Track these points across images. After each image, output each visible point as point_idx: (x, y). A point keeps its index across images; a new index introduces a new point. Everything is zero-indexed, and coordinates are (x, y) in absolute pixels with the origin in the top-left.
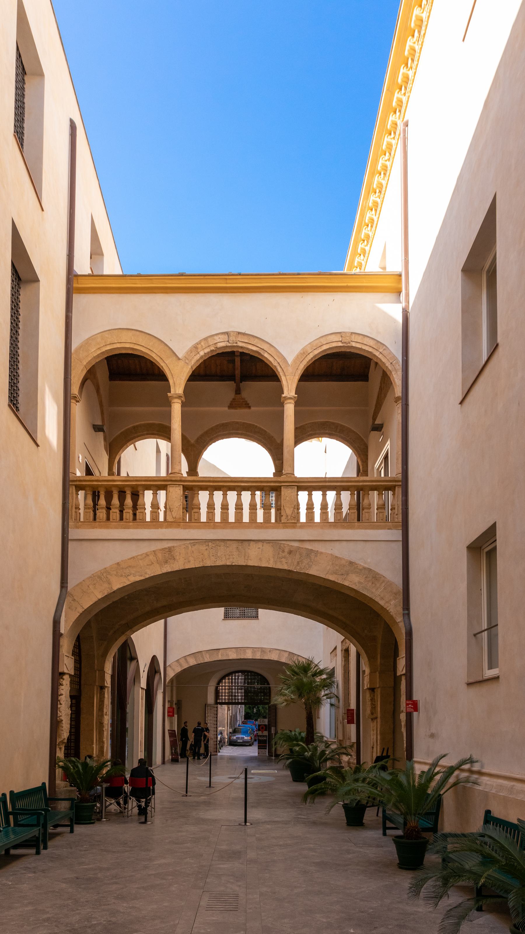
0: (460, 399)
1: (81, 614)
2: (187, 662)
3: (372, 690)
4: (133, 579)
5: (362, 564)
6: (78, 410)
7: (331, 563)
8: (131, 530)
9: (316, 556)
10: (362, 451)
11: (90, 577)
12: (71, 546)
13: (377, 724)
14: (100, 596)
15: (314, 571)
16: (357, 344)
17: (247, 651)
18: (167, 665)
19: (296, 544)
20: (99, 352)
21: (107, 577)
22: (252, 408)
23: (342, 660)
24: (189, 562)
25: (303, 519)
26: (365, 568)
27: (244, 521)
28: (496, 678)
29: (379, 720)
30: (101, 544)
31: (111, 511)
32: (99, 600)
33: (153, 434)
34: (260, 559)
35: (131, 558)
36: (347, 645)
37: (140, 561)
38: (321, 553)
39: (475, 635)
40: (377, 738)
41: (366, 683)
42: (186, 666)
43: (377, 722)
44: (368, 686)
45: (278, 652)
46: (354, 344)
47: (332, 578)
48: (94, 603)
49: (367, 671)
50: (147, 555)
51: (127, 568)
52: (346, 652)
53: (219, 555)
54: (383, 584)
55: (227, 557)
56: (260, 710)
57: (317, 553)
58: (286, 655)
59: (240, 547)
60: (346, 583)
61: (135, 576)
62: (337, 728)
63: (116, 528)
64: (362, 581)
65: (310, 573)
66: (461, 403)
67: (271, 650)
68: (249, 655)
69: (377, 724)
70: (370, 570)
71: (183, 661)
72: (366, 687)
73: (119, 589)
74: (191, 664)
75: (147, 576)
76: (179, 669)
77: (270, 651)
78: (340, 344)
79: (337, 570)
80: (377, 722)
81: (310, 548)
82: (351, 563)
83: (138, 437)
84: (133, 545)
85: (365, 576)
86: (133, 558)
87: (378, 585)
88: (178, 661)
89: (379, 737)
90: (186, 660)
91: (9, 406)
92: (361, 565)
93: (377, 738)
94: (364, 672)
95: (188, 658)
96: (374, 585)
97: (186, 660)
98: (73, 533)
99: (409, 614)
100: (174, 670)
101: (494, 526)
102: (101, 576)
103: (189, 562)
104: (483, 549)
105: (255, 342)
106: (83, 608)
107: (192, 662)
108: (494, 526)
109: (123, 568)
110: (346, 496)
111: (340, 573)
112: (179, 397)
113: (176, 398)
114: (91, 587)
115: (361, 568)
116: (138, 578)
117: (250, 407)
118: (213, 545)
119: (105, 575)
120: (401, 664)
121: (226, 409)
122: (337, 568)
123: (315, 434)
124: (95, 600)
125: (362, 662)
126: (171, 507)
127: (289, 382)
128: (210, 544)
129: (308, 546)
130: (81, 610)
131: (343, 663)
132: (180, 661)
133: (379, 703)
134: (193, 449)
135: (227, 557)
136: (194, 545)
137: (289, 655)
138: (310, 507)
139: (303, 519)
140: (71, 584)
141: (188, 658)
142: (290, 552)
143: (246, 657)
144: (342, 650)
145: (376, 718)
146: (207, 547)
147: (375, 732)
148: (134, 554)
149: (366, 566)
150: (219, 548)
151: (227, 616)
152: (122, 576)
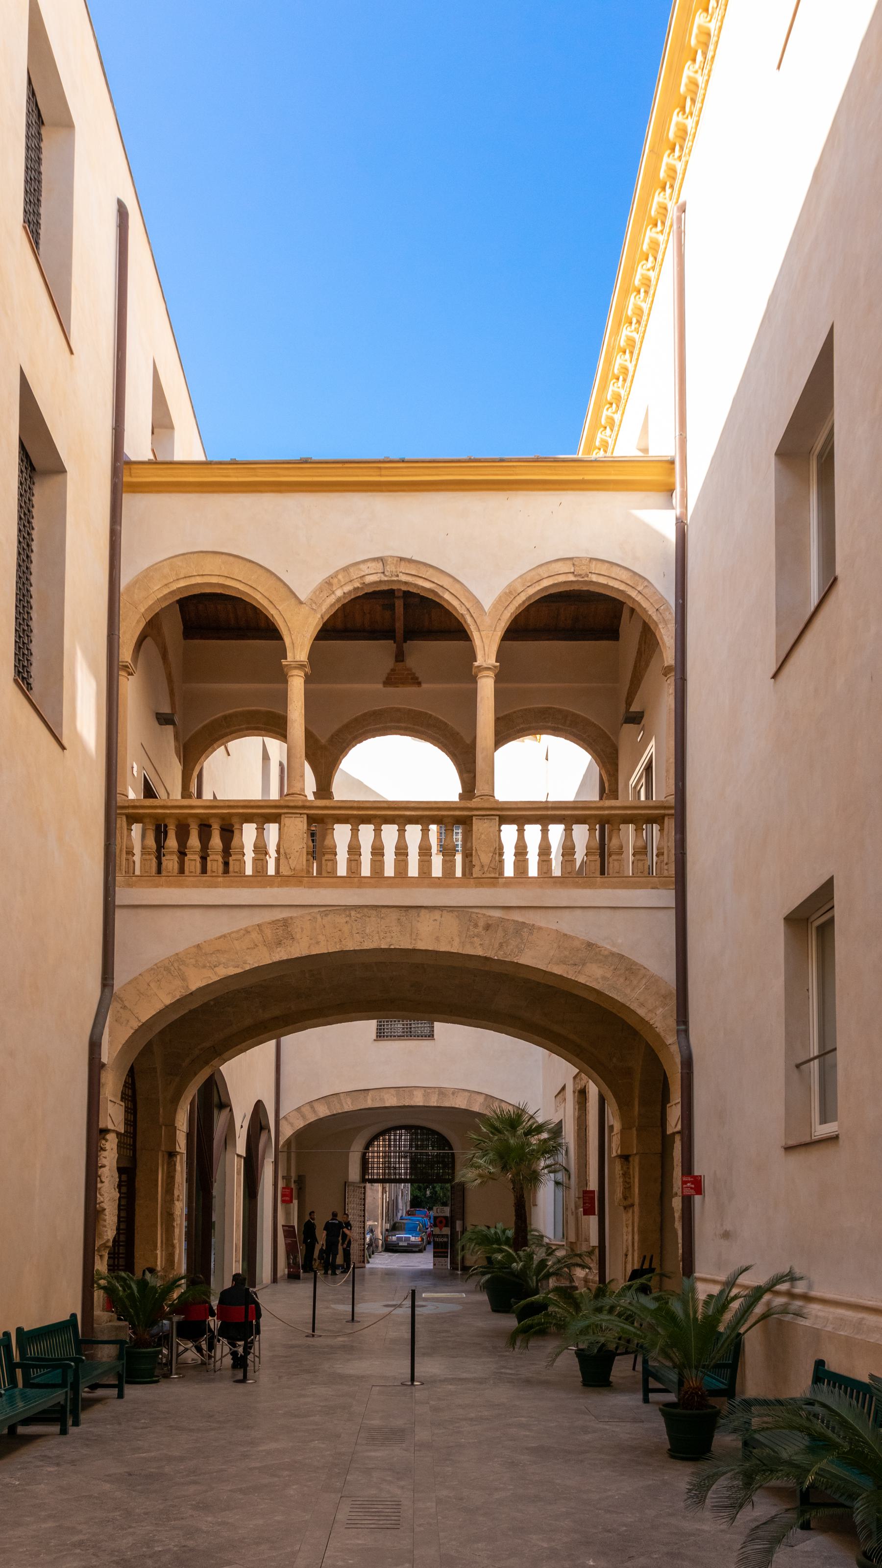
0: (774, 669)
1: (136, 1031)
2: (314, 1111)
3: (625, 1158)
4: (223, 972)
5: (608, 947)
6: (131, 688)
7: (555, 945)
8: (221, 890)
9: (531, 933)
10: (608, 758)
11: (152, 969)
12: (120, 916)
13: (633, 1216)
14: (168, 1001)
15: (527, 959)
16: (599, 578)
17: (415, 1093)
18: (281, 1116)
19: (497, 914)
20: (166, 591)
21: (180, 969)
22: (424, 686)
23: (575, 1109)
24: (318, 943)
25: (509, 871)
26: (613, 954)
27: (410, 875)
28: (833, 1139)
29: (636, 1208)
30: (170, 913)
31: (186, 858)
32: (167, 1007)
33: (257, 729)
34: (437, 939)
35: (220, 938)
36: (583, 1083)
37: (236, 942)
38: (540, 928)
39: (798, 1066)
40: (633, 1238)
41: (615, 1147)
42: (312, 1118)
43: (633, 1212)
44: (619, 1152)
45: (467, 1094)
46: (594, 578)
47: (557, 970)
48: (158, 1013)
49: (617, 1126)
50: (247, 931)
51: (213, 953)
52: (582, 1094)
53: (367, 931)
54: (644, 981)
55: (382, 935)
56: (436, 1192)
57: (532, 928)
58: (481, 1099)
59: (403, 919)
60: (582, 979)
61: (226, 966)
62: (567, 1222)
63: (195, 886)
64: (609, 975)
65: (521, 962)
66: (775, 676)
67: (455, 1092)
68: (418, 1100)
69: (633, 1216)
70: (621, 957)
71: (307, 1110)
72: (614, 1154)
73: (200, 989)
74: (322, 1115)
75: (247, 968)
76: (300, 1124)
77: (453, 1094)
78: (571, 578)
79: (566, 957)
80: (633, 1212)
81: (520, 919)
82: (590, 945)
83: (231, 733)
84: (224, 915)
85: (613, 967)
86: (224, 936)
87: (635, 982)
88: (298, 1109)
89: (636, 1237)
90: (312, 1107)
91: (16, 681)
92: (606, 949)
93: (633, 1238)
94: (611, 1128)
95: (316, 1105)
96: (628, 982)
97: (312, 1107)
98: (123, 896)
99: (686, 1031)
100: (292, 1125)
101: (830, 883)
102: (170, 967)
103: (318, 943)
104: (812, 921)
105: (428, 573)
106: (140, 1021)
107: (323, 1111)
108: (830, 883)
109: (206, 954)
110: (581, 833)
111: (572, 962)
112: (301, 666)
113: (296, 668)
114: (152, 985)
115: (606, 953)
116: (232, 971)
117: (419, 684)
118: (358, 915)
119: (176, 965)
120: (674, 1114)
121: (380, 686)
122: (567, 953)
123: (529, 729)
124: (159, 1007)
125: (608, 1111)
126: (288, 851)
127: (486, 641)
128: (353, 913)
129: (517, 916)
130: (136, 1025)
131: (576, 1114)
132: (303, 1109)
133: (637, 1180)
134: (325, 754)
135: (382, 935)
136: (326, 915)
137: (485, 1100)
138: (521, 851)
139: (509, 871)
140: (120, 980)
141: (316, 1105)
142: (487, 927)
143: (412, 1104)
144: (574, 1092)
145: (632, 1205)
146: (348, 919)
147: (630, 1229)
148: (226, 930)
149: (615, 950)
150: (367, 919)
151: (381, 1035)
152: (204, 967)
